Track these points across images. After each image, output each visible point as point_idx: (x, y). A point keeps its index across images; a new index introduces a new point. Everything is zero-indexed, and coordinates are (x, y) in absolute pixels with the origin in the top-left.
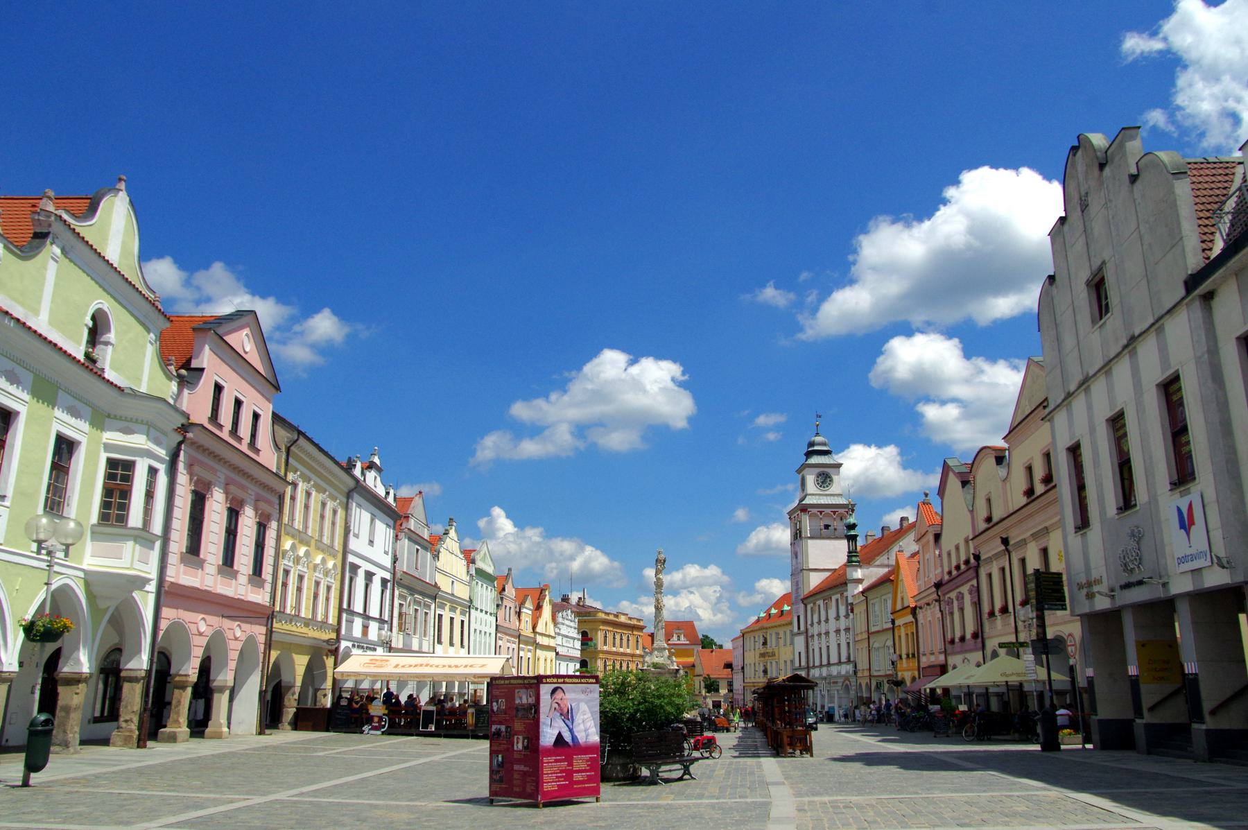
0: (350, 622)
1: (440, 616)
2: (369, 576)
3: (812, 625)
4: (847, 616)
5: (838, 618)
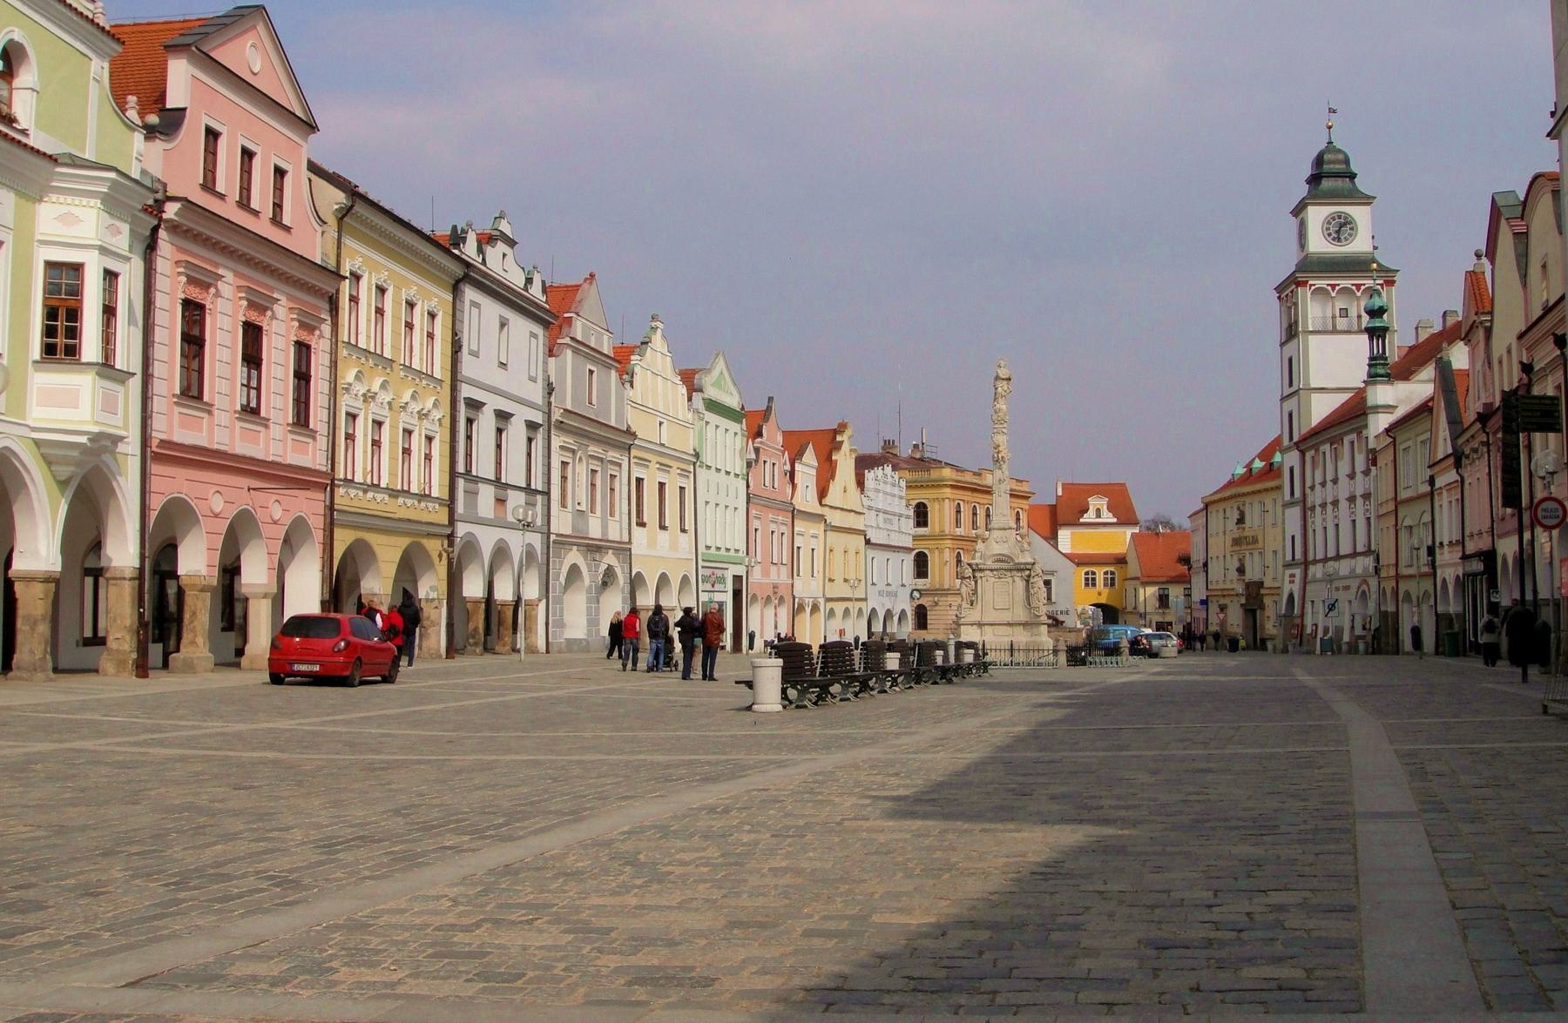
0: (472, 494)
1: (639, 481)
2: (503, 416)
3: (1312, 488)
4: (1366, 473)
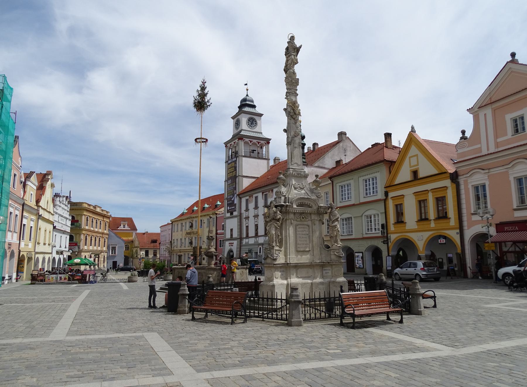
5: (256, 207)
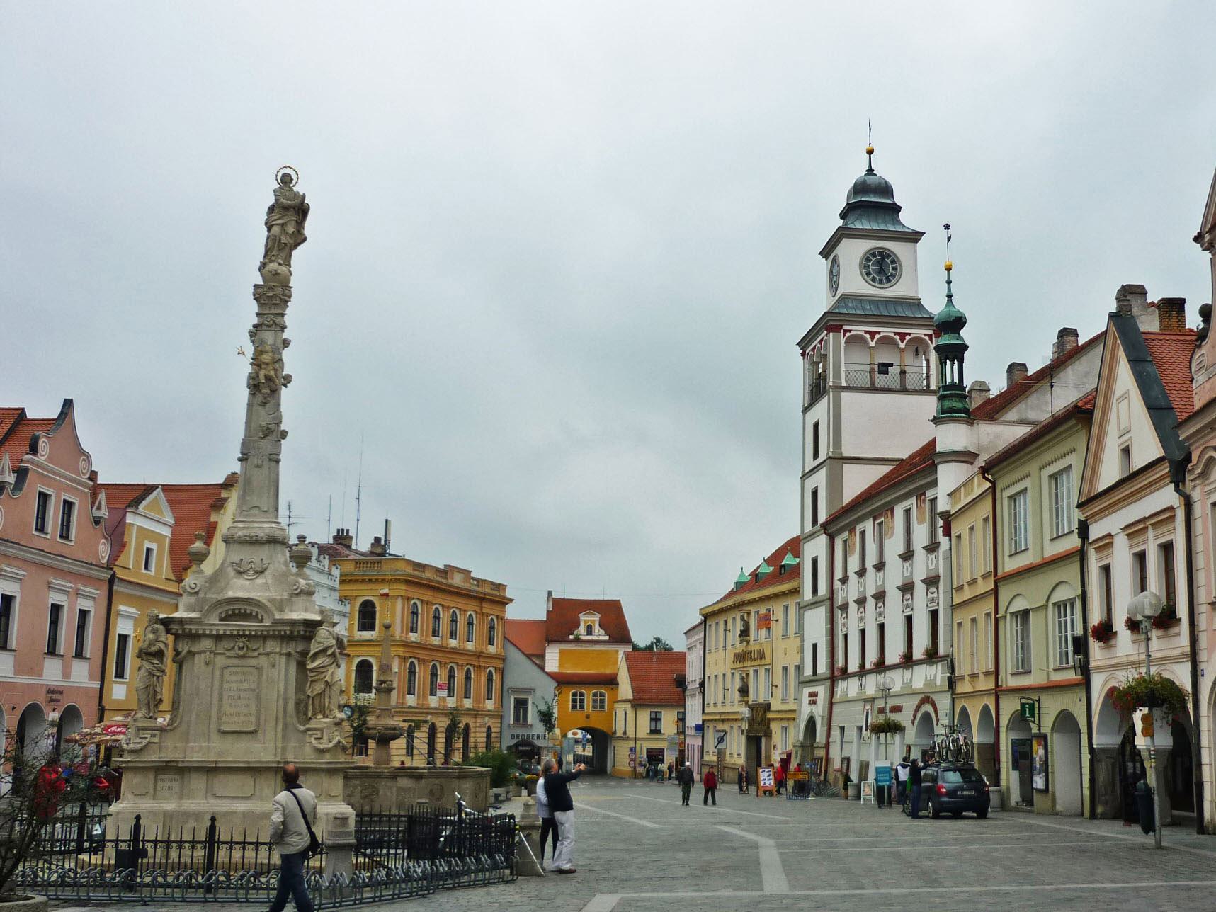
3: (844, 580)
4: (932, 548)
